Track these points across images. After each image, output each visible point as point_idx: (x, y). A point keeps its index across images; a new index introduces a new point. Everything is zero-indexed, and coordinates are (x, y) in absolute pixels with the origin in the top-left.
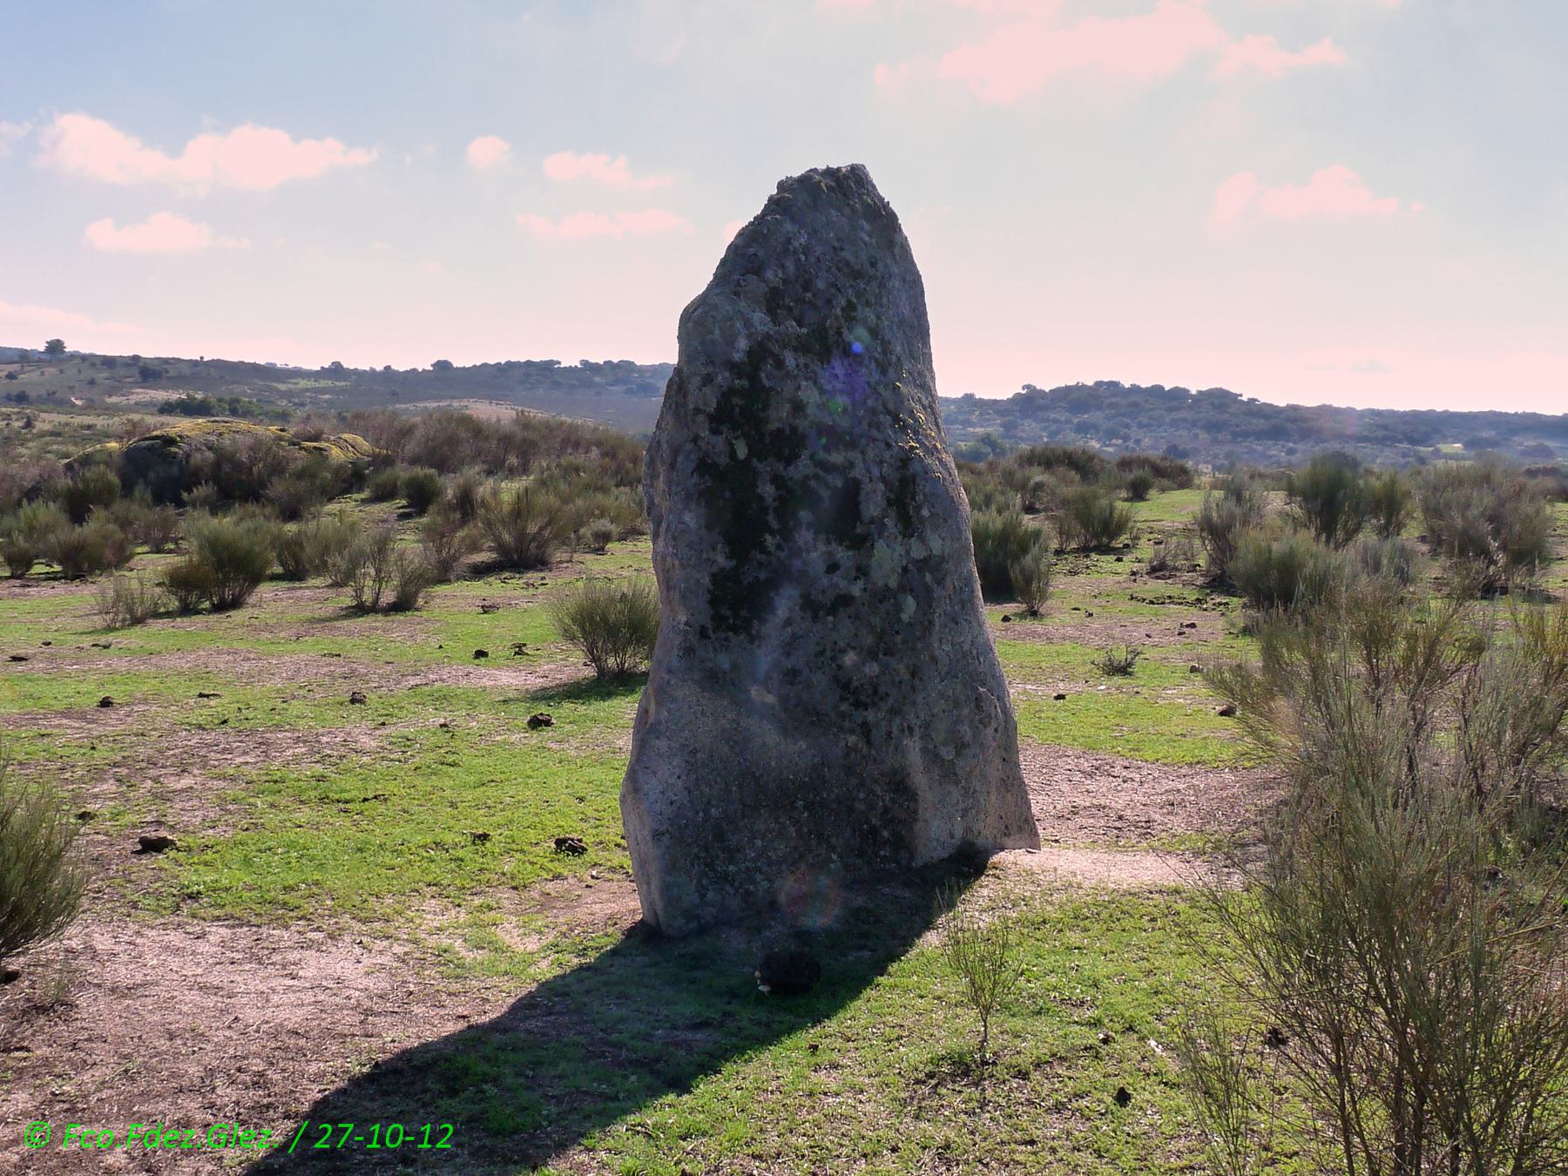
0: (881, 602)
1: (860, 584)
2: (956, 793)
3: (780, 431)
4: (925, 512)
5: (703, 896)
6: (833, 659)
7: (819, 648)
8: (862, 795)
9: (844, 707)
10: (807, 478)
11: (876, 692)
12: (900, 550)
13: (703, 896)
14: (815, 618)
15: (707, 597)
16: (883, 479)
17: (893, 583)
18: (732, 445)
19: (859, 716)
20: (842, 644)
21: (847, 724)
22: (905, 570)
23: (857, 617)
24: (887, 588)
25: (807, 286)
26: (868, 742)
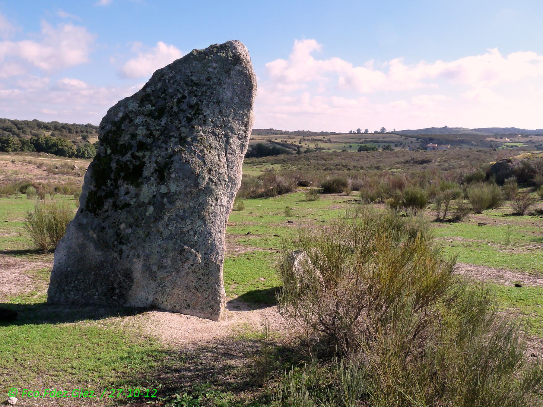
0: (140, 207)
1: (134, 200)
2: (153, 285)
3: (124, 145)
4: (173, 175)
5: (55, 294)
6: (118, 225)
7: (114, 221)
8: (113, 275)
9: (116, 243)
10: (128, 161)
11: (128, 239)
12: (154, 188)
13: (55, 294)
14: (115, 210)
15: (86, 199)
16: (156, 162)
17: (146, 201)
18: (106, 149)
19: (120, 247)
20: (121, 221)
21: (115, 249)
22: (154, 196)
23: (129, 212)
24: (144, 202)
25: (165, 91)
26: (120, 257)
